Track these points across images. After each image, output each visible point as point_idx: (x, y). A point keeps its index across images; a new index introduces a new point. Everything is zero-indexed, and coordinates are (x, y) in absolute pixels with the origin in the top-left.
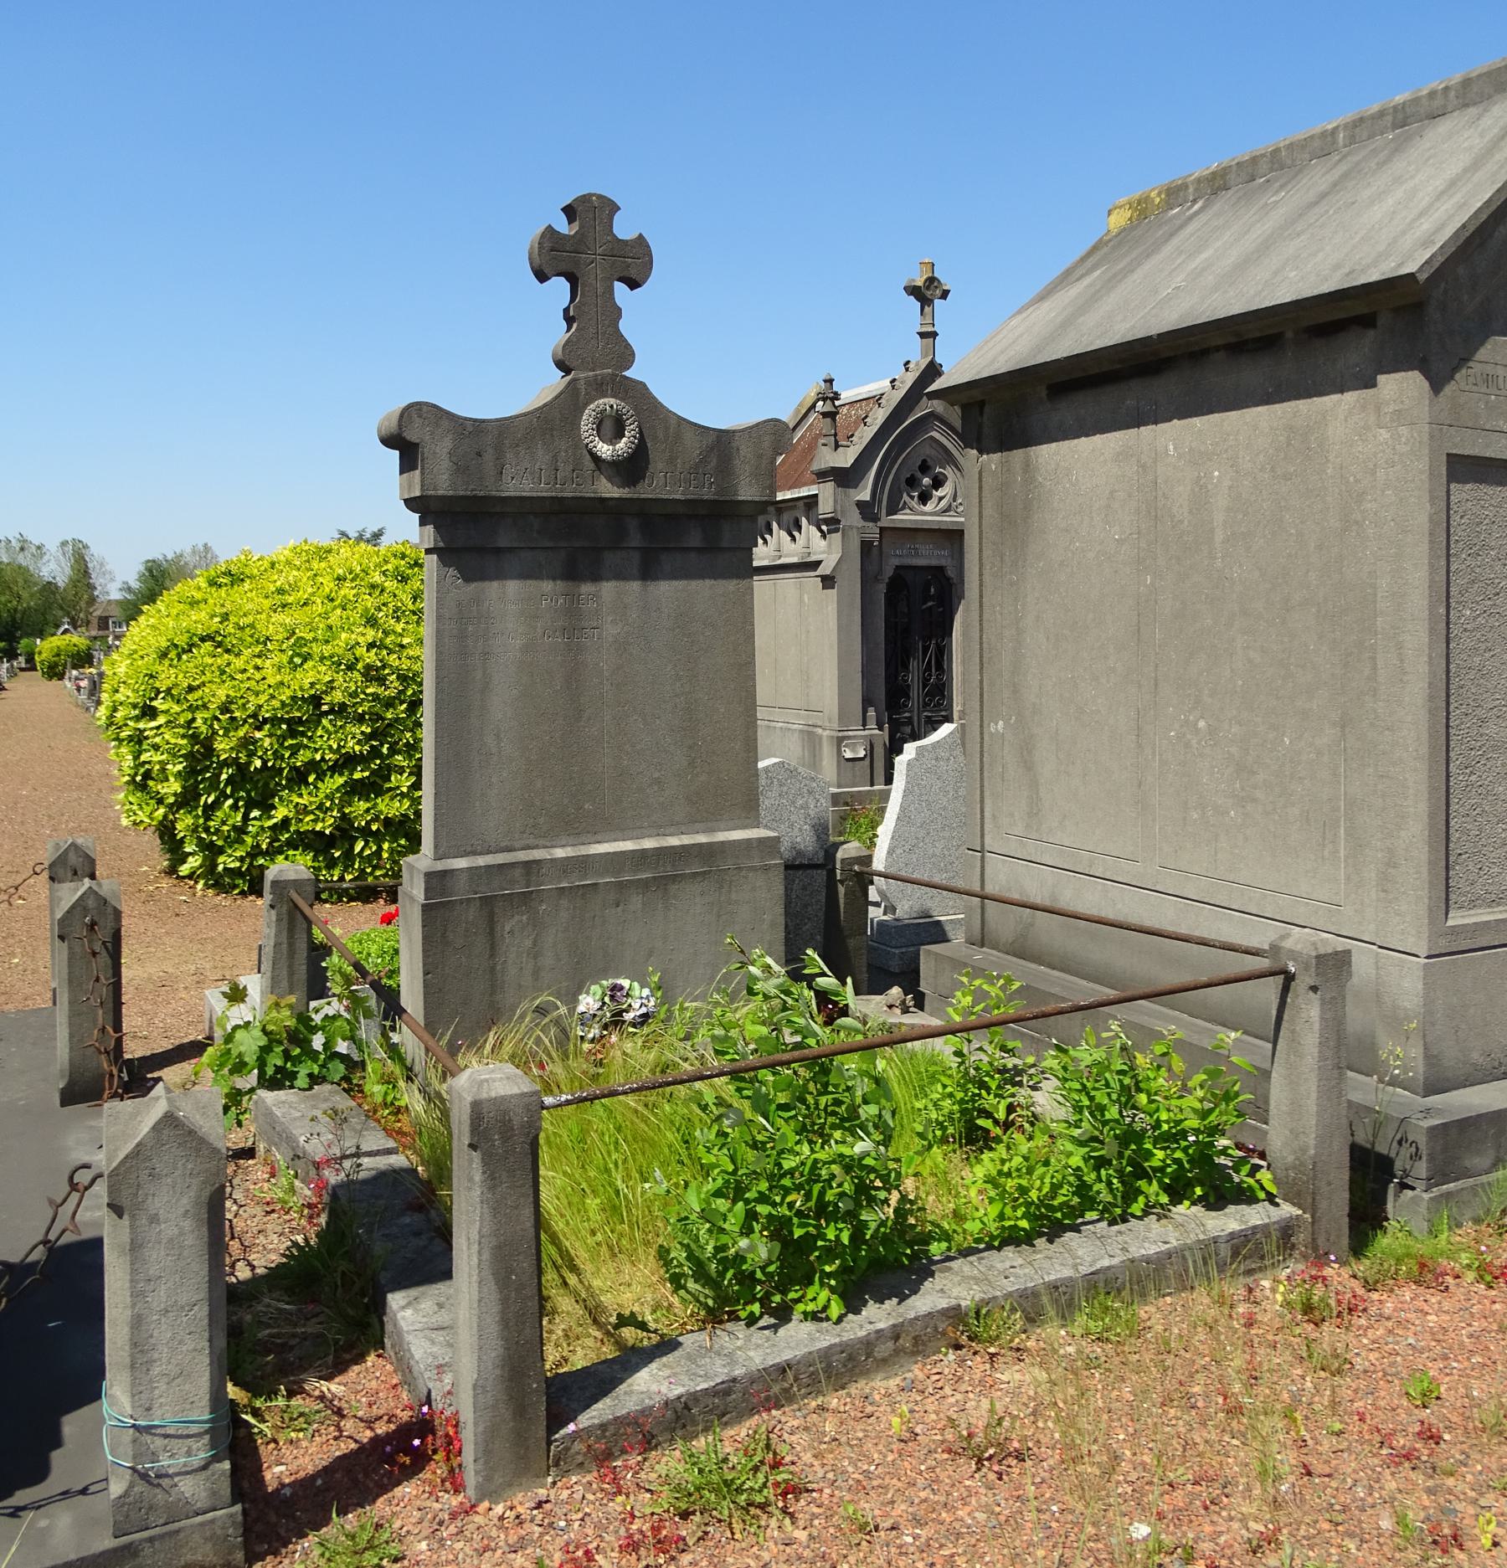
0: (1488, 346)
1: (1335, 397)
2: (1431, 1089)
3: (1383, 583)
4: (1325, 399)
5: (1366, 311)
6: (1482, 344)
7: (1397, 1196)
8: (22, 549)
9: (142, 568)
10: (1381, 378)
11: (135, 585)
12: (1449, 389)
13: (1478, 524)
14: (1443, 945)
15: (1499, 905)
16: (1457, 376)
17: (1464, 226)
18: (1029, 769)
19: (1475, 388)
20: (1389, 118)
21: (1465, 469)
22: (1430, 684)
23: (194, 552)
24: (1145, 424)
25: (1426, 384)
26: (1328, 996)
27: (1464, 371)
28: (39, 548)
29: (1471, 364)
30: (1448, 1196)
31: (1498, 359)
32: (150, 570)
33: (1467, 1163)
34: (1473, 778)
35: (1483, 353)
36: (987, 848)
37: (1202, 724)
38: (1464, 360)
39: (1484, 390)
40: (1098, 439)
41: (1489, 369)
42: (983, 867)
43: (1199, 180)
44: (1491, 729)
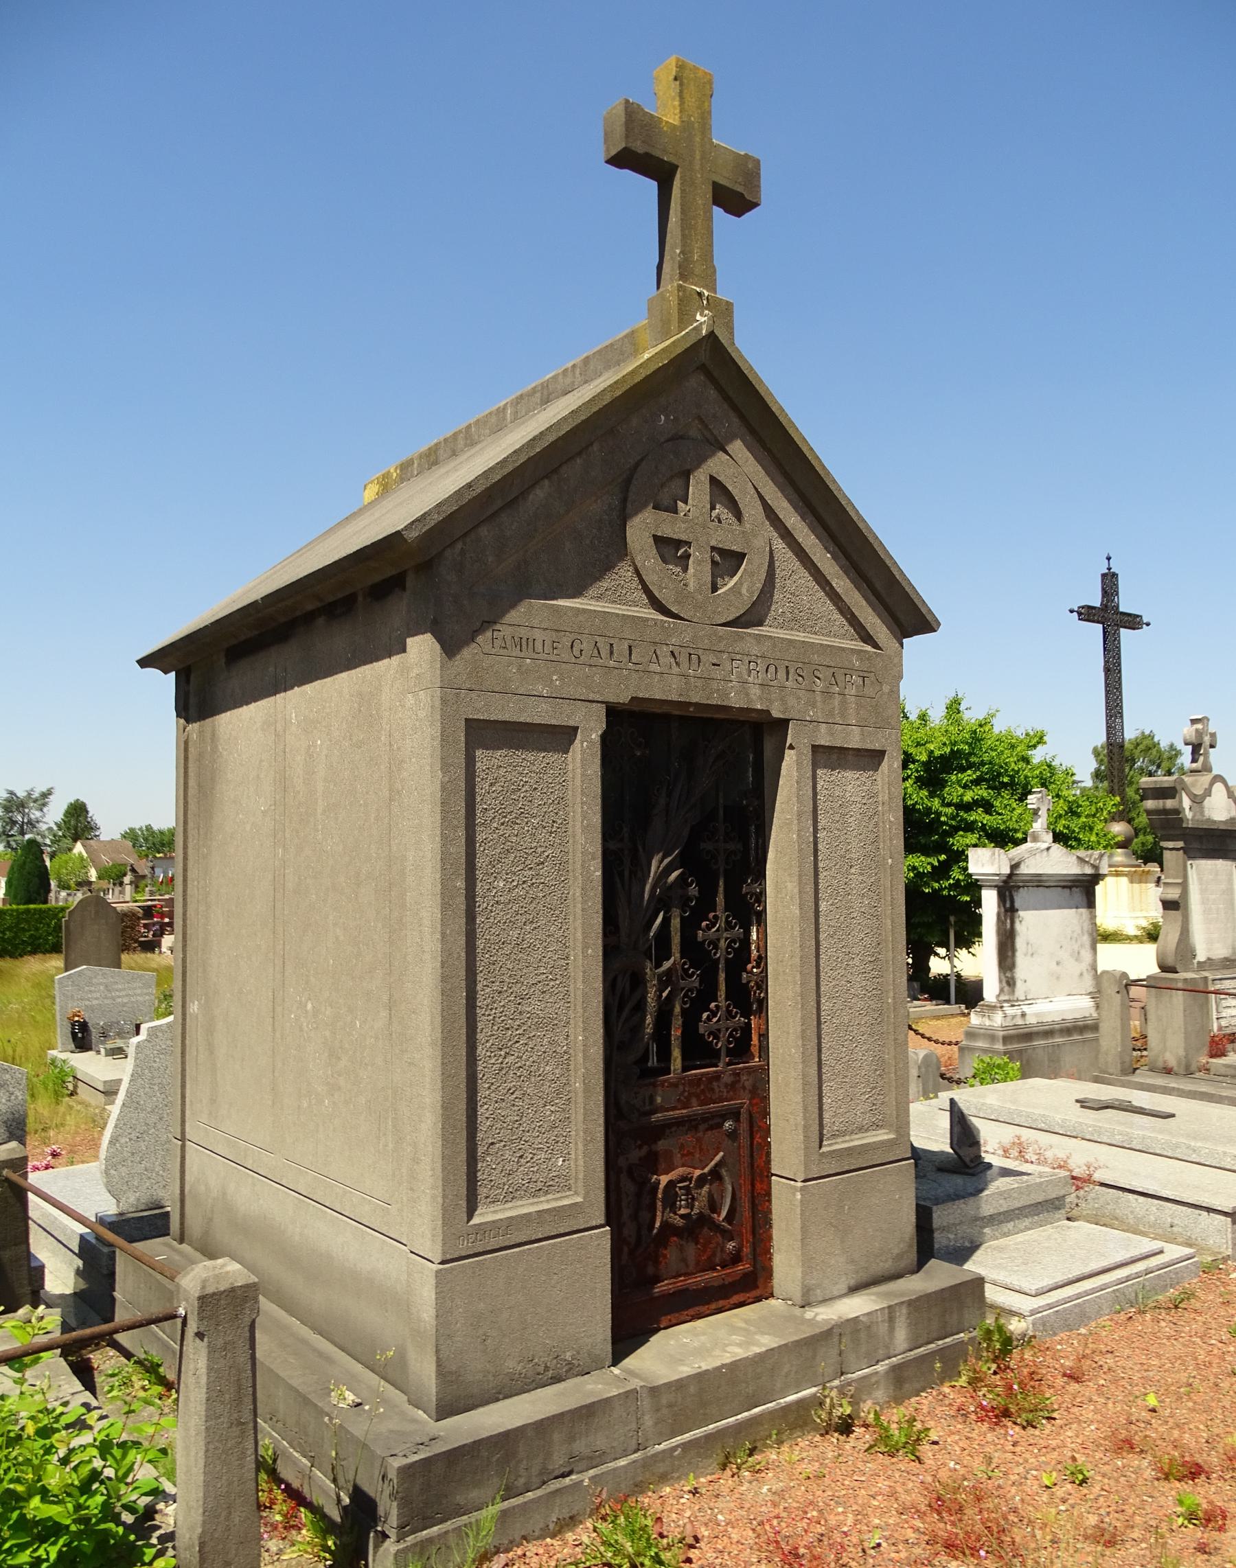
0: (522, 608)
1: (386, 661)
2: (445, 1410)
3: (410, 856)
4: (380, 663)
5: (394, 572)
6: (513, 605)
7: (376, 1547)
10: (409, 641)
12: (467, 653)
13: (514, 791)
14: (464, 1247)
15: (547, 1193)
16: (480, 639)
17: (469, 485)
18: (212, 1053)
19: (502, 652)
20: (538, 395)
21: (483, 734)
22: (443, 963)
24: (279, 692)
25: (438, 646)
26: (220, 1342)
27: (489, 634)
29: (498, 627)
30: (423, 1545)
31: (535, 623)
33: (459, 1499)
34: (510, 1059)
35: (513, 616)
36: (188, 1137)
37: (309, 1006)
38: (489, 623)
39: (516, 652)
40: (253, 706)
41: (523, 632)
42: (183, 1158)
43: (420, 457)
44: (533, 1006)
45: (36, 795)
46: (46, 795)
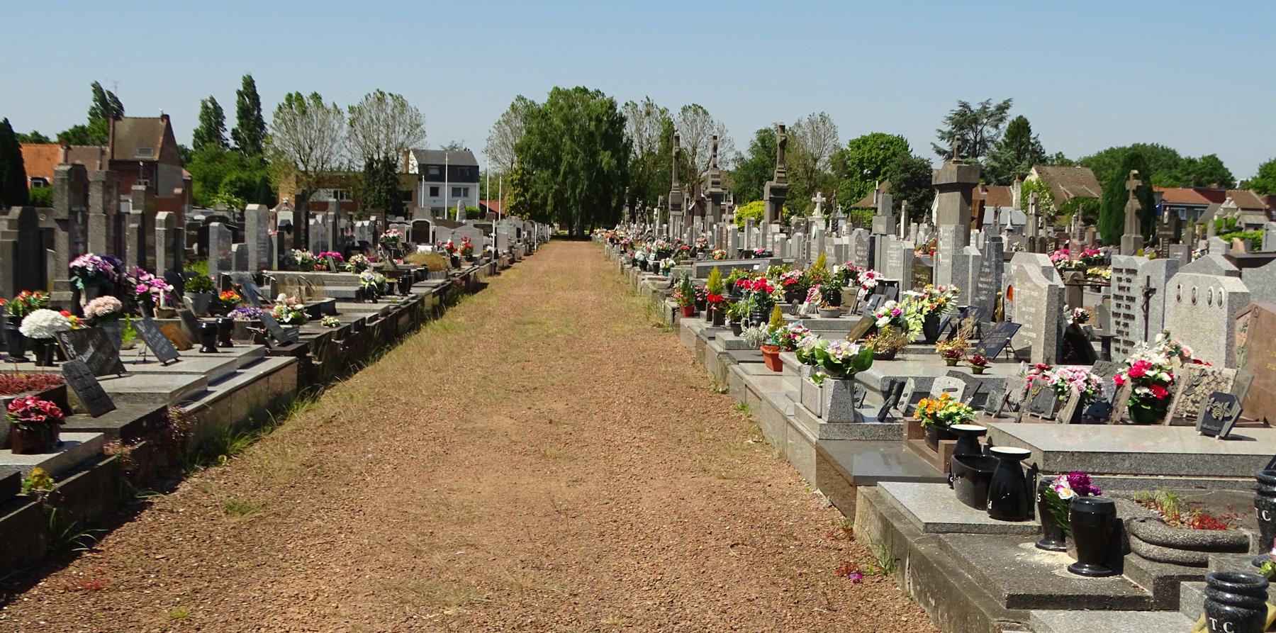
8: (648, 114)
9: (755, 138)
11: (748, 156)
23: (812, 122)
28: (662, 112)
32: (762, 140)
45: (992, 108)
46: (1003, 108)
